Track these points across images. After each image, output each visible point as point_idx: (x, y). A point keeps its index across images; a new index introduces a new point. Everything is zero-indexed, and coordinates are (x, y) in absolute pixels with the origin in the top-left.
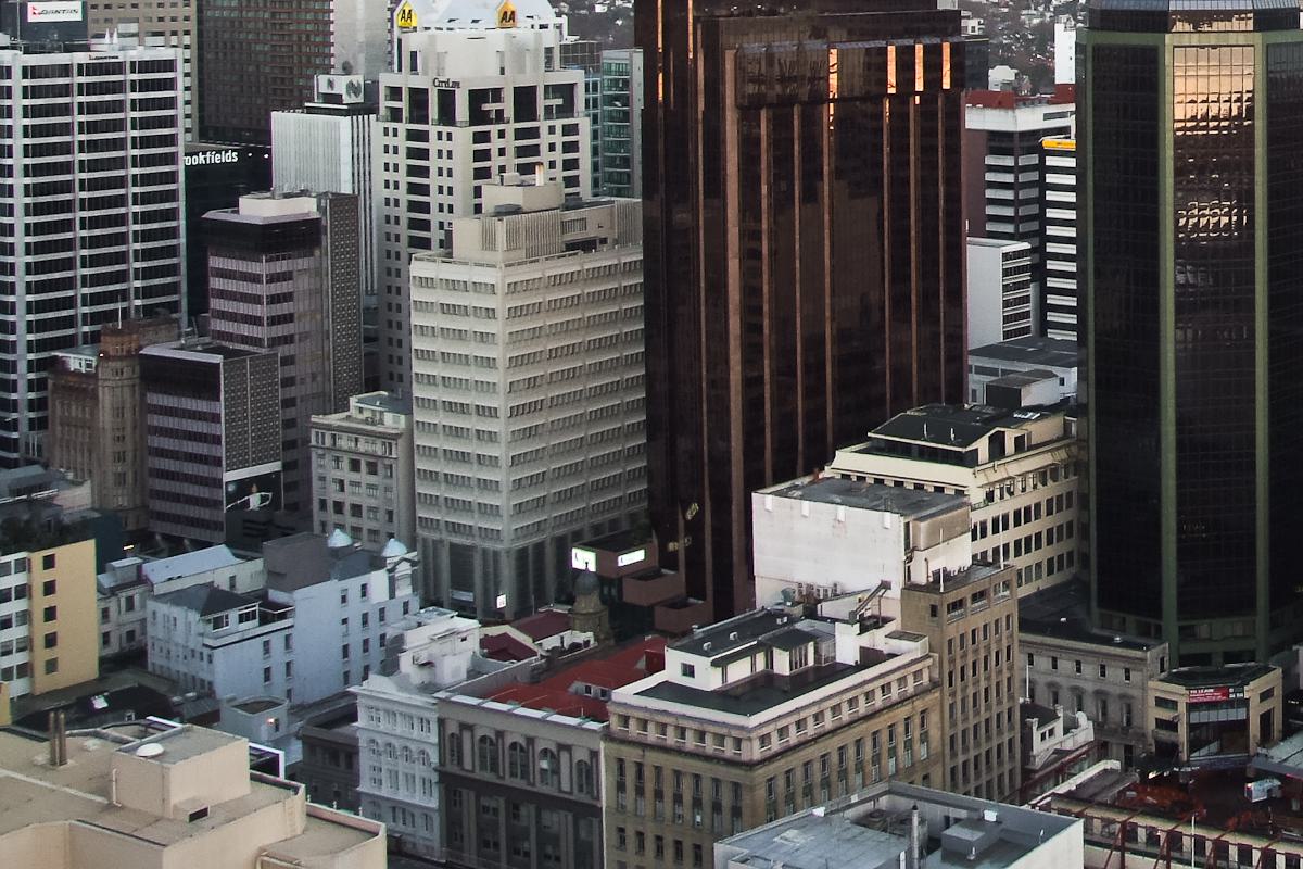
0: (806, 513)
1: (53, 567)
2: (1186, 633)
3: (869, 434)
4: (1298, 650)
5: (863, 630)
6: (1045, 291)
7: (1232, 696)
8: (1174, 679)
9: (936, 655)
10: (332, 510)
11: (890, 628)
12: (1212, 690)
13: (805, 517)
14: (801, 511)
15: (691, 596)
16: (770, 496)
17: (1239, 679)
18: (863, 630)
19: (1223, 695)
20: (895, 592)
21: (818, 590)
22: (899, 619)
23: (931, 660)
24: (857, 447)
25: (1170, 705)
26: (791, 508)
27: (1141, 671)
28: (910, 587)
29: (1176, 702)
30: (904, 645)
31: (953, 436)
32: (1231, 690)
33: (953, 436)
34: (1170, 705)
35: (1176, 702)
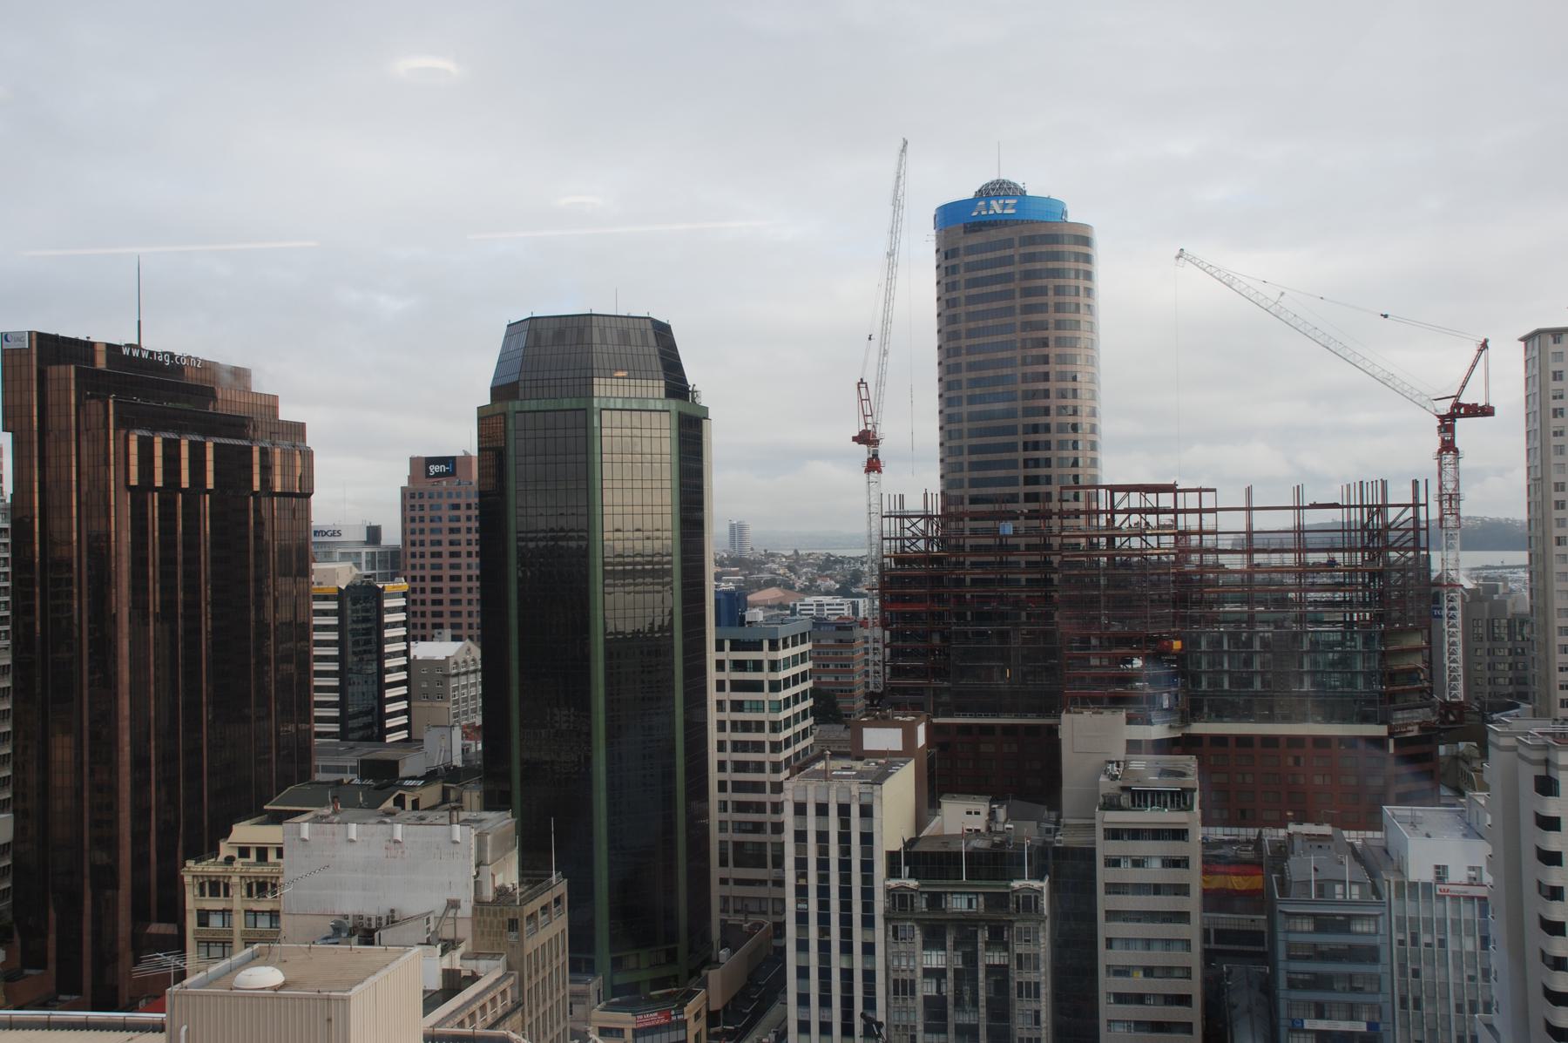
0: (353, 836)
1: (303, 425)
2: (617, 963)
3: (265, 807)
4: (707, 976)
5: (444, 951)
6: (340, 705)
7: (674, 1018)
8: (611, 1007)
9: (517, 973)
10: (968, 277)
11: (462, 948)
12: (656, 1014)
13: (352, 841)
14: (347, 835)
15: (61, 994)
16: (307, 824)
17: (676, 1001)
18: (444, 951)
19: (666, 1018)
20: (466, 909)
21: (370, 919)
22: (469, 940)
23: (512, 978)
24: (254, 820)
25: (614, 1033)
26: (334, 834)
27: (584, 1003)
28: (479, 903)
29: (623, 1030)
30: (482, 965)
31: (361, 799)
32: (673, 1012)
33: (361, 799)
34: (614, 1033)
35: (623, 1030)
